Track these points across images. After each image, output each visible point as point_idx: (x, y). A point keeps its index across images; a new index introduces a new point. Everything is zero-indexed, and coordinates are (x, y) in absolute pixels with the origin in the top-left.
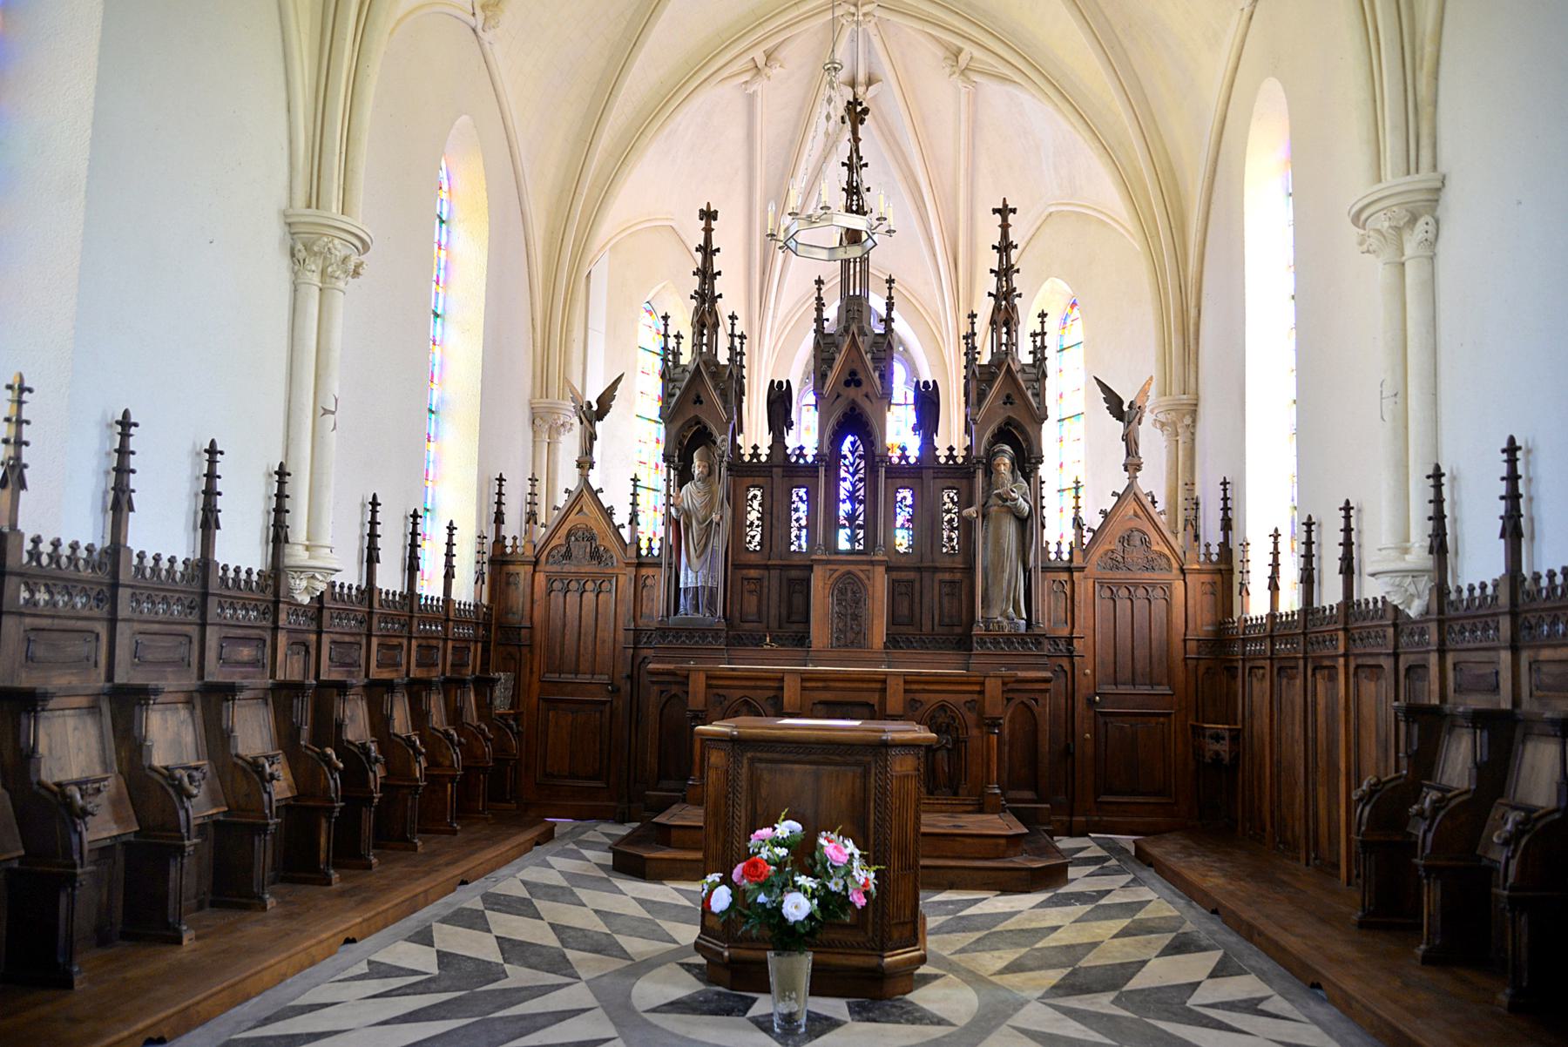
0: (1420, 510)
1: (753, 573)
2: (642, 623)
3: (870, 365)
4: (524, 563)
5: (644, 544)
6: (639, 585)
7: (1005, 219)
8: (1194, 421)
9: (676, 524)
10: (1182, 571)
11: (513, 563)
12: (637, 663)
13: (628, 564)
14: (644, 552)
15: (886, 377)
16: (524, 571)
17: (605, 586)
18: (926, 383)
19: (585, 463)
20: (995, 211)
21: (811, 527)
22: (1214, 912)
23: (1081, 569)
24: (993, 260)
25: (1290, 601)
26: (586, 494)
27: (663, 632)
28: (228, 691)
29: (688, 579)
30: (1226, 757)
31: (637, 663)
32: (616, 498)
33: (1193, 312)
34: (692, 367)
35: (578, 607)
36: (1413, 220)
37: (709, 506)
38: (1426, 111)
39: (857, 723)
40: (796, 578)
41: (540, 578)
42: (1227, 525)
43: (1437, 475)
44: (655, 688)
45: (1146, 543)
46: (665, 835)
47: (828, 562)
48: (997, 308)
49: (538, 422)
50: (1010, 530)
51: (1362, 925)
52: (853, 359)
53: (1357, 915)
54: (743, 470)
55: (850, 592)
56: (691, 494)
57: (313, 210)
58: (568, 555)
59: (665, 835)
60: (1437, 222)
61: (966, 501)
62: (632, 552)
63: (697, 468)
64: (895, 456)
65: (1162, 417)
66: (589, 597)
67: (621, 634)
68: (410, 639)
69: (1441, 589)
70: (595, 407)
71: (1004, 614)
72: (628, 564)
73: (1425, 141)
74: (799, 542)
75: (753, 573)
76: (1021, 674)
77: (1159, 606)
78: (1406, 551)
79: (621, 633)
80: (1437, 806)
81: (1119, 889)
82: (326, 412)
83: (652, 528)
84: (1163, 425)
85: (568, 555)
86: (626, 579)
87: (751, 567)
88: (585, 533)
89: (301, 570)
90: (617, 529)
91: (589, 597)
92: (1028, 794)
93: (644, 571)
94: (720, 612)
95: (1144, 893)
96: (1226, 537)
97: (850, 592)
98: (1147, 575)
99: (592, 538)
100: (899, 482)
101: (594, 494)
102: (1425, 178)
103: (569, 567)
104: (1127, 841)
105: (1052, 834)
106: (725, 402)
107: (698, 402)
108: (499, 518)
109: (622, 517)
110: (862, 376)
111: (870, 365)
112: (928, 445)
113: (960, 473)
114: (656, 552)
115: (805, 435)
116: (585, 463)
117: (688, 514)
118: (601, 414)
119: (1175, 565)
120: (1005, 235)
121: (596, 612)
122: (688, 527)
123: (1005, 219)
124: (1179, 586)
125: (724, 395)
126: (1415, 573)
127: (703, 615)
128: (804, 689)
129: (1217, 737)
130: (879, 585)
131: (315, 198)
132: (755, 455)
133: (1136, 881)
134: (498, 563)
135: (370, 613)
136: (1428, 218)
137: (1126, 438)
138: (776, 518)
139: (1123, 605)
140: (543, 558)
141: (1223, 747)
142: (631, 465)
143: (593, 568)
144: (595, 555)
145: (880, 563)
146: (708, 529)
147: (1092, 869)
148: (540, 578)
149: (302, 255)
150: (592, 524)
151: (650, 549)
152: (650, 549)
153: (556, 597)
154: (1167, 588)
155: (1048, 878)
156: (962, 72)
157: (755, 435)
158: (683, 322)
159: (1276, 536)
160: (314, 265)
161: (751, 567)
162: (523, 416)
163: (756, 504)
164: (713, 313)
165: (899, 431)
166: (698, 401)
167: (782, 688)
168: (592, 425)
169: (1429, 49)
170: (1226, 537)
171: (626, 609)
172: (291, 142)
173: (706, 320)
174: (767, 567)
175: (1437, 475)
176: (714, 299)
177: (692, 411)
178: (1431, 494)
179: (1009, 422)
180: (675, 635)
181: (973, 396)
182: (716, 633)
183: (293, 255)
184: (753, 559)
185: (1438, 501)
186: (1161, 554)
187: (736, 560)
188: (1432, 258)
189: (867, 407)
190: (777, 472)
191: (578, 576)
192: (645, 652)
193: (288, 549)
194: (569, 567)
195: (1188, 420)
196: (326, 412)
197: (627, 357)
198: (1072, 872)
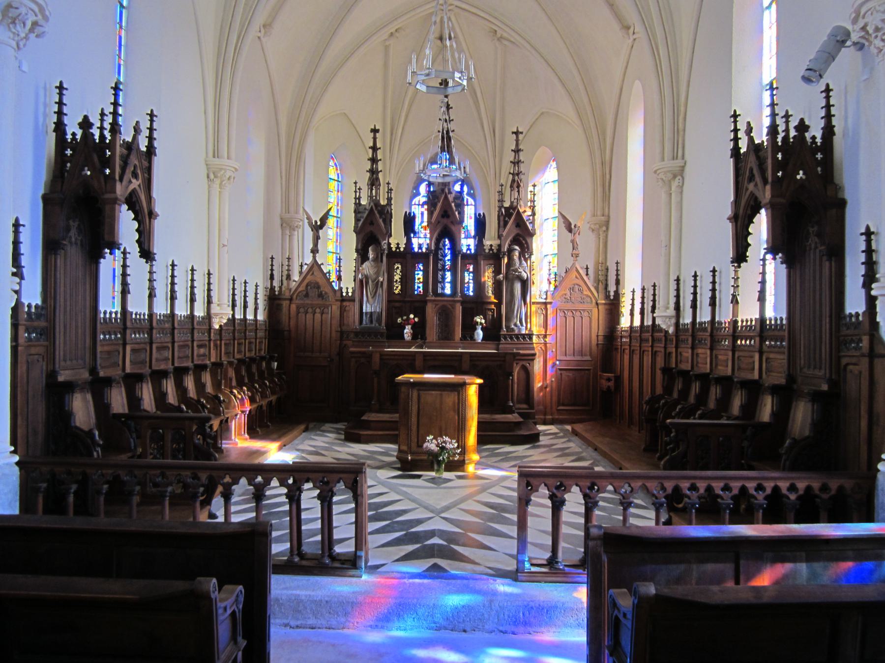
0: (673, 293)
1: (397, 305)
2: (344, 328)
3: (454, 208)
4: (285, 299)
5: (344, 291)
6: (342, 310)
7: (517, 137)
8: (607, 229)
9: (361, 284)
10: (597, 304)
11: (279, 299)
12: (342, 349)
13: (337, 300)
14: (344, 294)
15: (461, 213)
16: (285, 304)
17: (326, 310)
18: (480, 215)
19: (315, 251)
20: (513, 133)
21: (425, 283)
22: (596, 450)
23: (550, 303)
24: (511, 157)
25: (637, 323)
26: (315, 266)
27: (356, 334)
28: (108, 382)
29: (367, 308)
30: (613, 389)
31: (342, 349)
32: (329, 266)
33: (608, 176)
34: (368, 207)
35: (312, 321)
36: (675, 177)
37: (377, 274)
38: (681, 133)
39: (453, 376)
40: (418, 305)
41: (293, 307)
42: (618, 282)
43: (678, 280)
44: (353, 360)
45: (581, 291)
46: (367, 425)
47: (434, 301)
48: (513, 181)
49: (284, 225)
50: (518, 287)
51: (645, 450)
52: (445, 212)
53: (643, 447)
54: (394, 256)
55: (445, 314)
56: (368, 268)
57: (216, 159)
58: (307, 295)
59: (367, 425)
60: (683, 178)
61: (497, 272)
62: (338, 294)
63: (371, 255)
64: (464, 249)
65: (593, 226)
66: (318, 316)
67: (334, 334)
68: (245, 339)
69: (677, 324)
70: (319, 223)
71: (515, 325)
72: (337, 300)
73: (680, 146)
74: (419, 287)
75: (397, 305)
76: (521, 352)
77: (586, 320)
78: (668, 308)
79: (334, 334)
80: (664, 405)
81: (560, 443)
82: (224, 246)
83: (348, 285)
84: (593, 230)
85: (307, 295)
86: (335, 308)
87: (397, 301)
88: (315, 284)
89: (217, 315)
90: (331, 284)
91: (318, 316)
92: (525, 406)
93: (345, 304)
94: (383, 324)
95: (571, 444)
96: (617, 288)
97: (445, 314)
98: (581, 305)
99: (319, 287)
100: (467, 261)
101: (319, 266)
102: (679, 162)
103: (308, 301)
104: (569, 427)
105: (536, 424)
106: (385, 224)
107: (371, 226)
108: (272, 277)
109: (333, 277)
110: (450, 213)
111: (454, 208)
112: (480, 245)
113: (495, 257)
114: (350, 294)
115: (422, 241)
116: (315, 251)
117: (367, 277)
118: (322, 226)
119: (594, 301)
120: (517, 145)
121: (321, 322)
122: (367, 283)
123: (517, 137)
124: (595, 310)
125: (384, 221)
126: (670, 317)
127: (375, 324)
128: (424, 360)
129: (609, 380)
130: (459, 310)
131: (216, 154)
132: (398, 248)
133: (569, 441)
134: (274, 300)
135: (234, 330)
136: (679, 177)
137: (573, 241)
138: (407, 280)
139: (570, 320)
140: (295, 297)
141: (611, 384)
142: (337, 256)
143: (320, 301)
144: (321, 295)
145: (458, 301)
146: (377, 284)
147: (567, 451)
148: (293, 307)
149: (212, 176)
150: (319, 280)
151: (347, 293)
152: (347, 293)
153: (302, 316)
154: (590, 312)
155: (533, 439)
156: (498, 39)
157: (397, 239)
158: (364, 183)
159: (633, 292)
160: (218, 181)
161: (397, 301)
162: (279, 222)
163: (398, 271)
164: (377, 179)
165: (467, 244)
166: (372, 223)
167: (415, 360)
168: (318, 232)
169: (682, 109)
170: (617, 288)
171: (336, 322)
172: (206, 127)
173: (374, 182)
174: (404, 302)
175: (678, 280)
176: (377, 172)
177: (371, 228)
178: (675, 287)
179: (518, 235)
180: (366, 334)
181: (502, 223)
182: (382, 335)
183: (208, 177)
184: (398, 298)
185: (678, 290)
186: (587, 296)
187: (391, 298)
188: (681, 193)
189: (453, 228)
190: (409, 256)
191: (312, 306)
192: (345, 342)
193: (212, 305)
194: (308, 301)
195: (604, 228)
196: (224, 246)
197: (335, 195)
198: (541, 438)
